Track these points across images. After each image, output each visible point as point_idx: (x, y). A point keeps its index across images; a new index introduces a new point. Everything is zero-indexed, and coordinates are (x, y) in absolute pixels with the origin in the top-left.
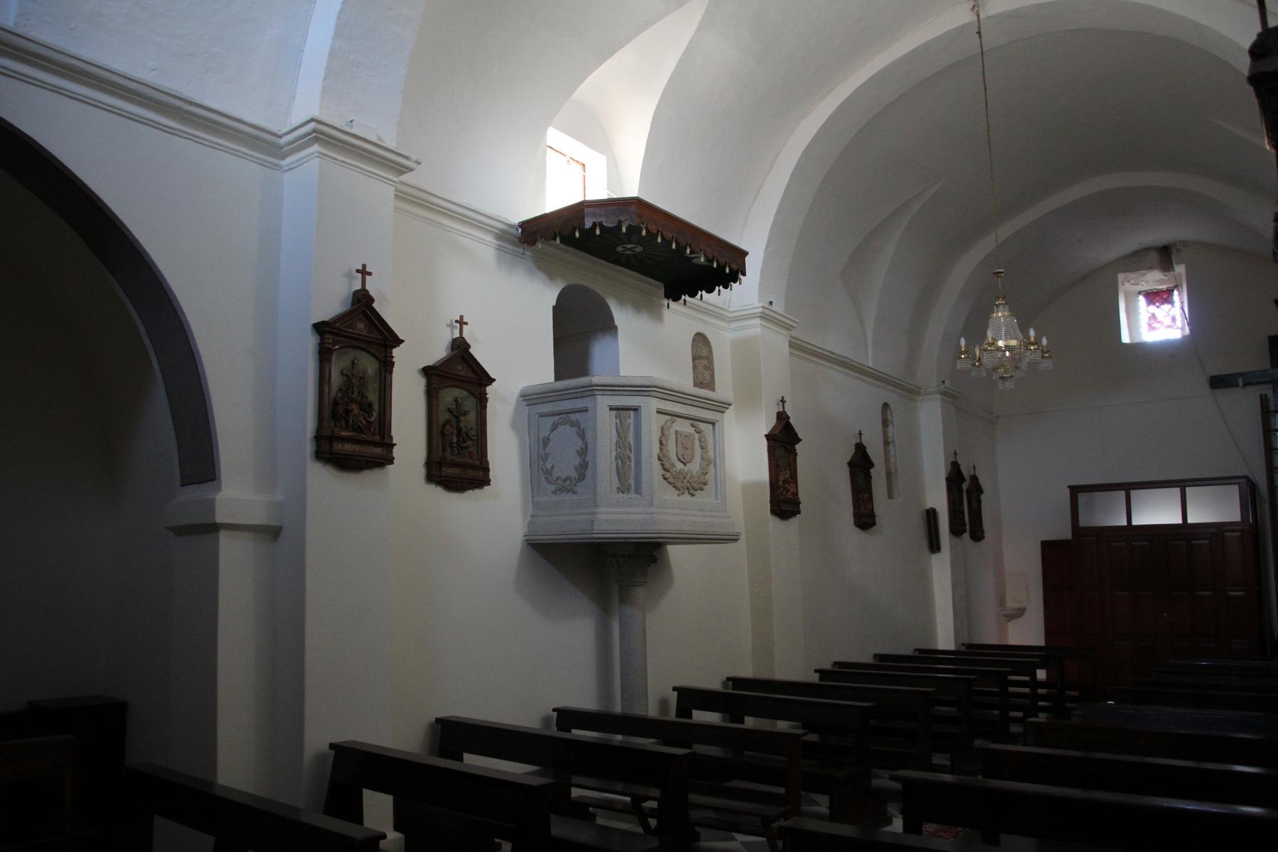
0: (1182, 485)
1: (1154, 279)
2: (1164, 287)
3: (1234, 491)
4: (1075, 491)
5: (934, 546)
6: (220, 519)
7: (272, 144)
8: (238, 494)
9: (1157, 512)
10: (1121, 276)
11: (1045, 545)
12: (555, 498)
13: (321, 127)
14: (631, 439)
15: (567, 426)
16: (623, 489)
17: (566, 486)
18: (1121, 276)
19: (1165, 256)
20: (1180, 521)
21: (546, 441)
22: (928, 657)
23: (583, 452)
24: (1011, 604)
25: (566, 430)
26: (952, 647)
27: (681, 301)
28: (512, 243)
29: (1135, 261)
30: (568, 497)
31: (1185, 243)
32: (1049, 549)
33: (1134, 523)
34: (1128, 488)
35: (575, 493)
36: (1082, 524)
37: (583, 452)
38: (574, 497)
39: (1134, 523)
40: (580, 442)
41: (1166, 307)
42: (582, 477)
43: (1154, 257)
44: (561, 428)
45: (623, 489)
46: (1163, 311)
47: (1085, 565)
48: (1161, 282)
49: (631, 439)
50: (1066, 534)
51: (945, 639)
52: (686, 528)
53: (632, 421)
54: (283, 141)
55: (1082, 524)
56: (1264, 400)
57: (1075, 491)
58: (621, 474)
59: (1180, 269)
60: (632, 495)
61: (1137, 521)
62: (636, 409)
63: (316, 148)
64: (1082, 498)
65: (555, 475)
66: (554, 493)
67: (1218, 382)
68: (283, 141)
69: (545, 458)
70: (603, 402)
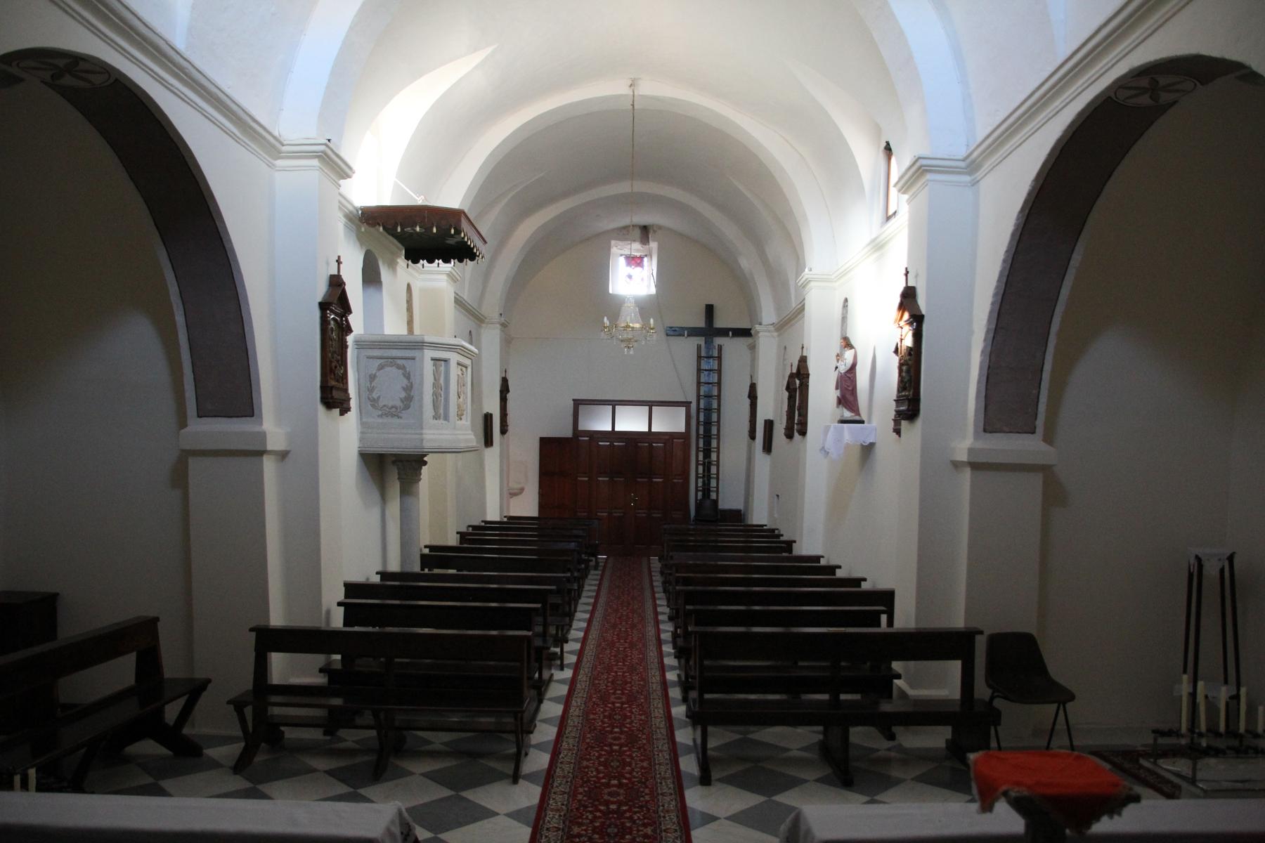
0: (651, 404)
1: (636, 248)
2: (638, 254)
3: (682, 411)
4: (578, 403)
5: (488, 442)
6: (269, 448)
7: (273, 146)
8: (273, 427)
9: (631, 422)
10: (613, 242)
11: (542, 439)
12: (380, 420)
13: (329, 152)
14: (442, 381)
15: (394, 369)
16: (436, 417)
17: (392, 412)
18: (613, 242)
19: (645, 232)
20: (646, 430)
21: (373, 378)
22: (489, 526)
23: (408, 389)
24: (515, 486)
25: (392, 371)
26: (497, 519)
27: (419, 265)
28: (346, 216)
29: (623, 233)
30: (396, 421)
31: (660, 227)
32: (547, 445)
33: (617, 429)
34: (614, 404)
35: (399, 417)
36: (580, 428)
37: (408, 389)
38: (401, 421)
39: (617, 429)
40: (405, 381)
41: (639, 269)
42: (407, 407)
43: (638, 232)
44: (388, 369)
45: (436, 417)
46: (636, 271)
47: (564, 458)
48: (638, 250)
49: (442, 381)
50: (568, 433)
51: (493, 514)
52: (444, 445)
53: (442, 369)
54: (284, 149)
55: (580, 428)
56: (699, 347)
57: (578, 403)
58: (435, 407)
59: (654, 245)
60: (442, 421)
61: (619, 427)
62: (445, 361)
63: (315, 162)
64: (581, 407)
65: (381, 404)
66: (380, 416)
67: (675, 332)
68: (284, 149)
69: (371, 390)
70: (429, 354)
